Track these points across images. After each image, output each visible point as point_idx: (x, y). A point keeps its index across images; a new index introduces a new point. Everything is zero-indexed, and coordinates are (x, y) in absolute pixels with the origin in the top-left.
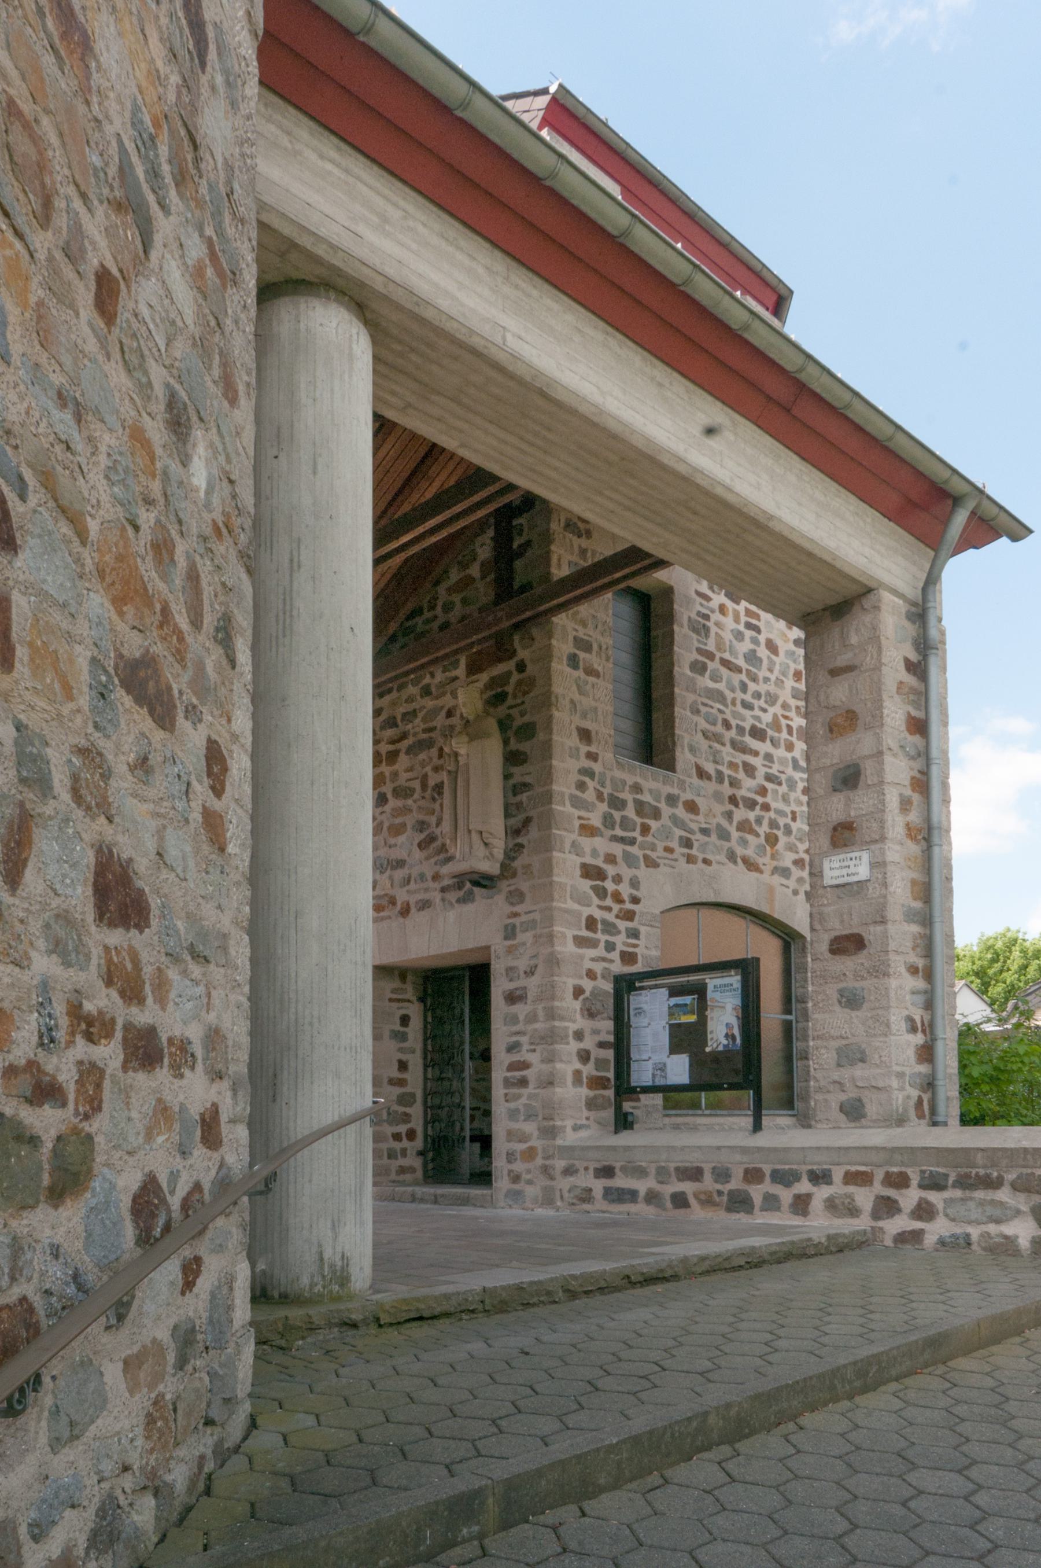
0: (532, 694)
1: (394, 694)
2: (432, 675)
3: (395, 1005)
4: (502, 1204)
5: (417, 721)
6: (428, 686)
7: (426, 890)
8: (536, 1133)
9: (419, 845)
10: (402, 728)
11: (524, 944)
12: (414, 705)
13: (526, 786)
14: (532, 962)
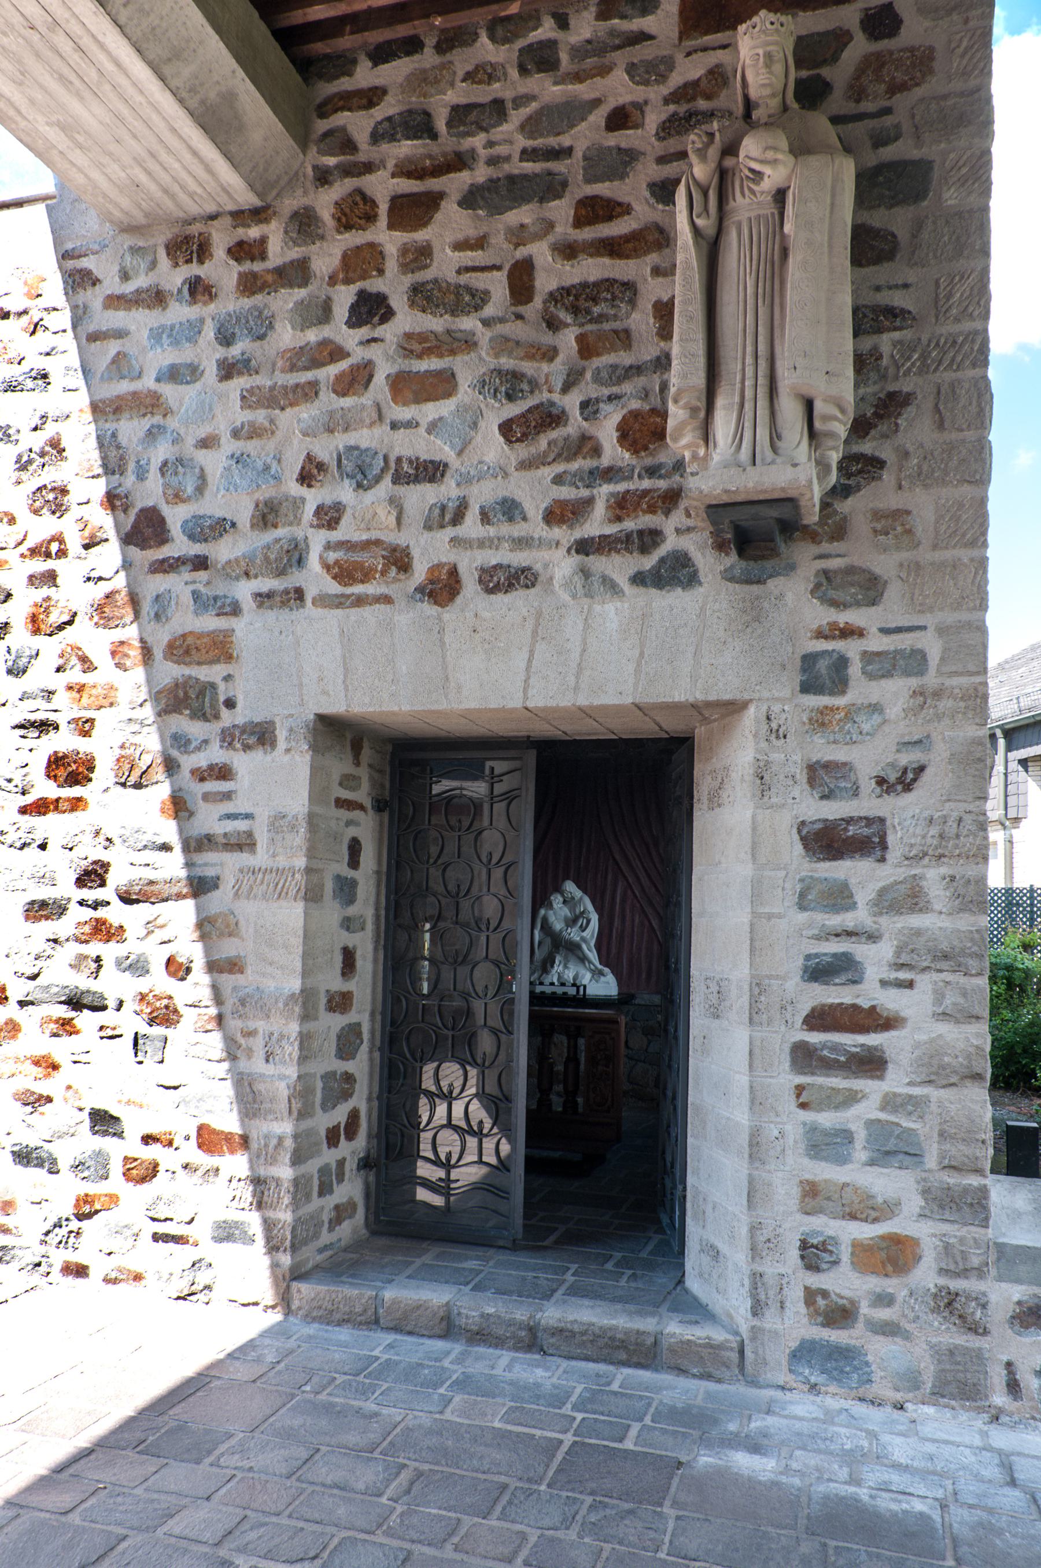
0: (918, 92)
1: (428, 58)
2: (563, 23)
3: (344, 814)
4: (783, 1377)
5: (508, 128)
6: (551, 45)
7: (522, 543)
8: (914, 1203)
9: (506, 429)
10: (447, 143)
11: (876, 708)
12: (496, 90)
13: (893, 316)
14: (905, 759)
